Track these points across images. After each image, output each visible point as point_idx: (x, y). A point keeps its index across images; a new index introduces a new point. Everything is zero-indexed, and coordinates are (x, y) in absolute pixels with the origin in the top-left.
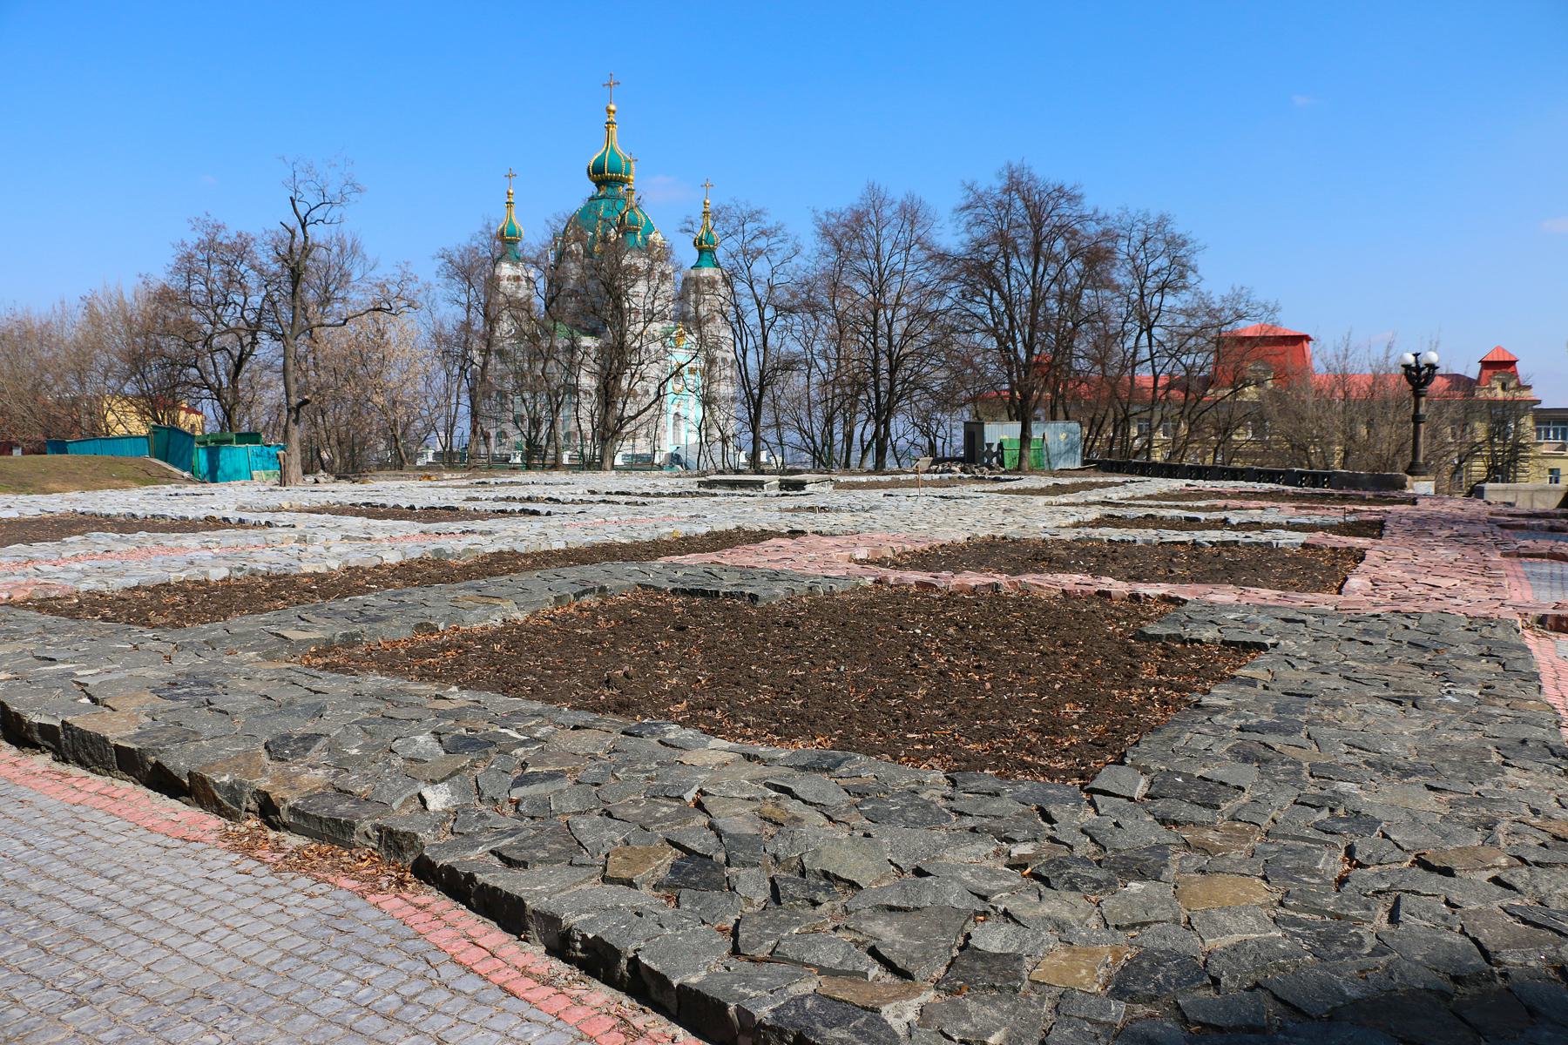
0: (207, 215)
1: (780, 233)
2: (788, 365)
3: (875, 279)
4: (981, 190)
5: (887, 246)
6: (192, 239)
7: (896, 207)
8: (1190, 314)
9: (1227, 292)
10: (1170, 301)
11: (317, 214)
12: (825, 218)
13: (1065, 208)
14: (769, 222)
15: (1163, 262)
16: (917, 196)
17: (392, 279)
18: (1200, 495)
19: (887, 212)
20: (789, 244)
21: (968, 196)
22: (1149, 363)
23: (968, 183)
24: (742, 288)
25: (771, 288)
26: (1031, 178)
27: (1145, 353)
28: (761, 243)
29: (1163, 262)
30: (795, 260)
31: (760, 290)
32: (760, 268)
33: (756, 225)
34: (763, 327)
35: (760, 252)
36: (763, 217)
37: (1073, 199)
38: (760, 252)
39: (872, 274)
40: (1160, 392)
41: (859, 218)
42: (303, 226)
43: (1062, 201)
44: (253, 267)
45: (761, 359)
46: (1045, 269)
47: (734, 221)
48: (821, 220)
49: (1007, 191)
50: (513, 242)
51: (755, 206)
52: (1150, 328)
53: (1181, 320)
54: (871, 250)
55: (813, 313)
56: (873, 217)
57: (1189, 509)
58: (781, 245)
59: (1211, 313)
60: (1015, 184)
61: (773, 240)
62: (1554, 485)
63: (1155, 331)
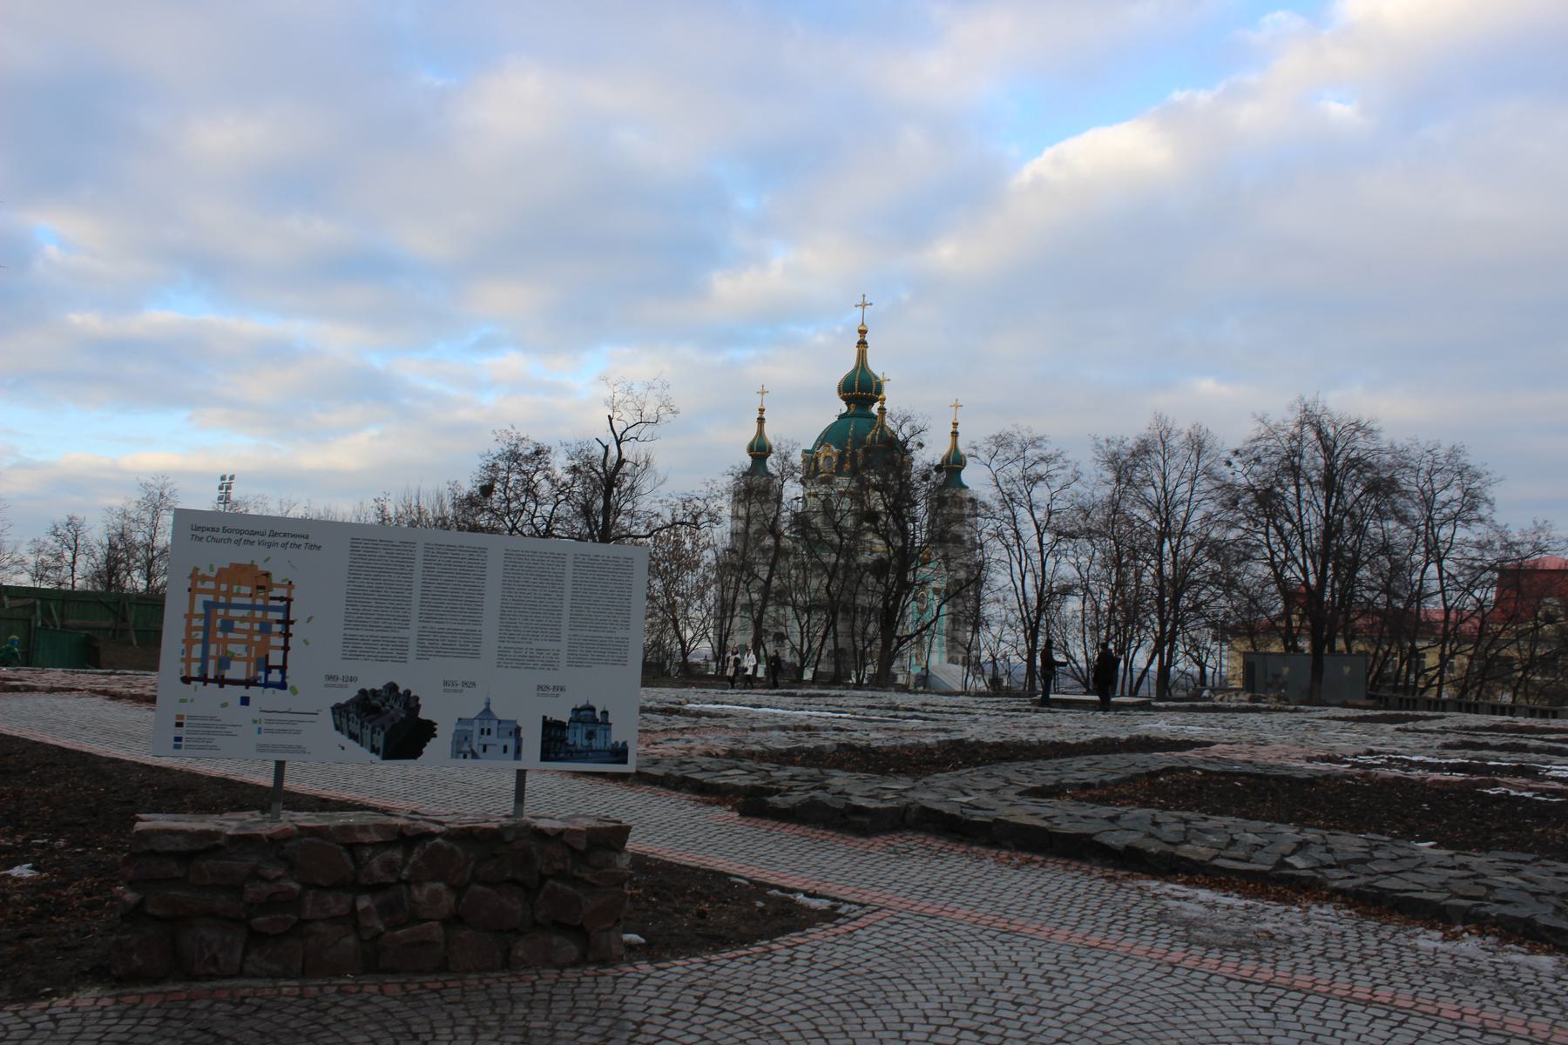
0: (513, 427)
1: (1060, 460)
2: (1066, 591)
3: (1161, 509)
4: (1272, 423)
5: (1173, 476)
6: (497, 449)
7: (1183, 437)
8: (1480, 546)
9: (1528, 525)
10: (1461, 533)
11: (631, 433)
12: (1105, 444)
13: (1362, 443)
14: (1049, 450)
15: (1454, 492)
16: (1204, 428)
17: (697, 494)
18: (1552, 731)
19: (1174, 442)
20: (1069, 471)
21: (1259, 428)
22: (1440, 595)
23: (1259, 415)
24: (1022, 513)
25: (1050, 513)
26: (1325, 408)
27: (1435, 585)
28: (1041, 469)
29: (1454, 492)
30: (1075, 486)
31: (1039, 515)
32: (1040, 493)
33: (1037, 451)
34: (1042, 551)
35: (1040, 478)
36: (1045, 445)
37: (1369, 432)
38: (1040, 478)
39: (1159, 502)
40: (1450, 627)
41: (1144, 449)
42: (618, 443)
43: (1357, 434)
44: (547, 477)
45: (1039, 583)
46: (1337, 501)
47: (1017, 447)
48: (1101, 447)
49: (1301, 424)
50: (1293, 435)
51: (1037, 433)
52: (1439, 562)
53: (1475, 553)
54: (1158, 479)
55: (1090, 539)
56: (1159, 447)
57: (1542, 739)
58: (1060, 471)
59: (1509, 546)
60: (1311, 420)
61: (1052, 466)
62: (280, 757)
63: (1445, 563)
